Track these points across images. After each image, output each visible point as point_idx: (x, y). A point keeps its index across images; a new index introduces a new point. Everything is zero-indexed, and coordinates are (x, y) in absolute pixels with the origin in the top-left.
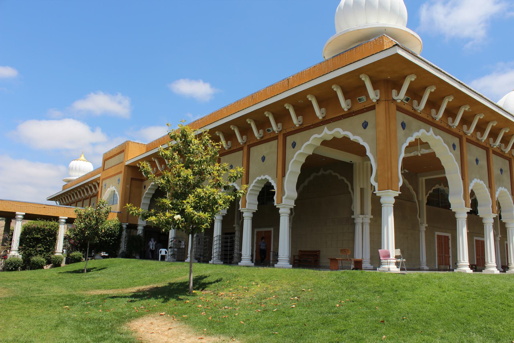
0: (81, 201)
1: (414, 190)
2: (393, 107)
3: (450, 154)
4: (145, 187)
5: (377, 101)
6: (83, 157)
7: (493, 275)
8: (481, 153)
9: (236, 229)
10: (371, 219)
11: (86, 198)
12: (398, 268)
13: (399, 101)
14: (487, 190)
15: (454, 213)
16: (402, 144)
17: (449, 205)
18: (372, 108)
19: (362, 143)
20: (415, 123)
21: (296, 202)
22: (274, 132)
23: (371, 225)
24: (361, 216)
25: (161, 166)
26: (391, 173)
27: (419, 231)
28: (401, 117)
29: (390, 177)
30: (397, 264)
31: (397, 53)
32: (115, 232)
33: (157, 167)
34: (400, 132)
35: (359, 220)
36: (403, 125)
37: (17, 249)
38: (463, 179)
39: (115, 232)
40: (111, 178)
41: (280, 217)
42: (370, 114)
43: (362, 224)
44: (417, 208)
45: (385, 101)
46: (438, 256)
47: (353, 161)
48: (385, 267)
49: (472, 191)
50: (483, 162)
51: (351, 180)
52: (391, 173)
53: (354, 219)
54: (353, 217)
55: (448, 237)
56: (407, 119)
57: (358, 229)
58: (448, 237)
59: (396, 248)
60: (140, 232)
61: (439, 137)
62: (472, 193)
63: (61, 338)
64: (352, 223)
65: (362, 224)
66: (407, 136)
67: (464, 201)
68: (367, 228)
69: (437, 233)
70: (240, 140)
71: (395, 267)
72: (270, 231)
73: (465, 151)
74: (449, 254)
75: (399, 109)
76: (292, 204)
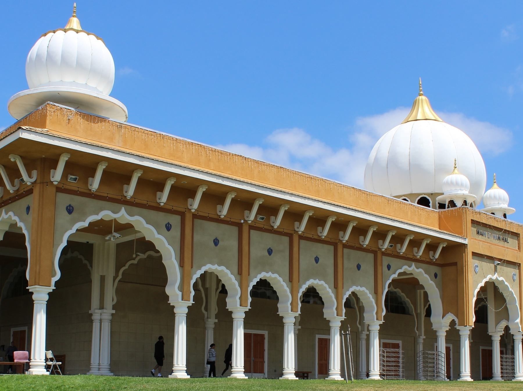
5: (32, 183)
12: (48, 371)
15: (173, 307)
17: (167, 297)
18: (30, 192)
24: (100, 311)
26: (40, 267)
27: (205, 328)
28: (64, 199)
29: (38, 271)
30: (48, 367)
34: (63, 216)
35: (96, 317)
37: (106, 361)
40: (194, 226)
42: (30, 197)
43: (101, 320)
44: (202, 298)
45: (40, 183)
46: (319, 364)
47: (91, 242)
52: (40, 267)
54: (114, 312)
55: (262, 336)
56: (76, 200)
57: (96, 326)
58: (262, 336)
59: (47, 349)
65: (101, 320)
71: (45, 370)
72: (25, 331)
74: (263, 357)
75: (59, 189)
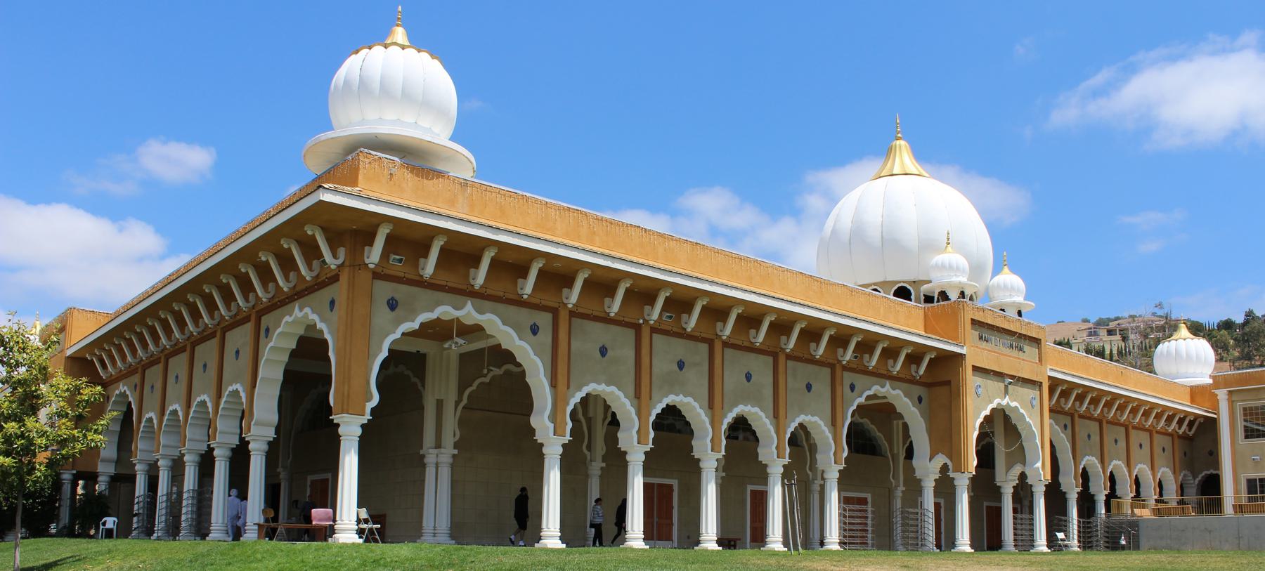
0: (183, 350)
2: (365, 277)
4: (267, 330)
5: (339, 266)
6: (400, 34)
7: (775, 554)
9: (281, 476)
10: (454, 456)
11: (153, 362)
13: (371, 266)
16: (387, 335)
18: (335, 279)
19: (327, 336)
20: (424, 295)
23: (453, 466)
24: (436, 451)
25: (287, 278)
28: (384, 290)
31: (321, 201)
32: (42, 489)
33: (275, 280)
35: (430, 459)
39: (42, 489)
41: (249, 456)
42: (335, 287)
43: (437, 464)
48: (703, 546)
51: (422, 379)
53: (423, 456)
54: (456, 452)
56: (401, 291)
57: (430, 473)
60: (103, 488)
64: (419, 463)
65: (437, 464)
66: (399, 322)
67: (551, 426)
68: (445, 473)
70: (328, 256)
72: (327, 480)
75: (377, 275)
76: (270, 434)
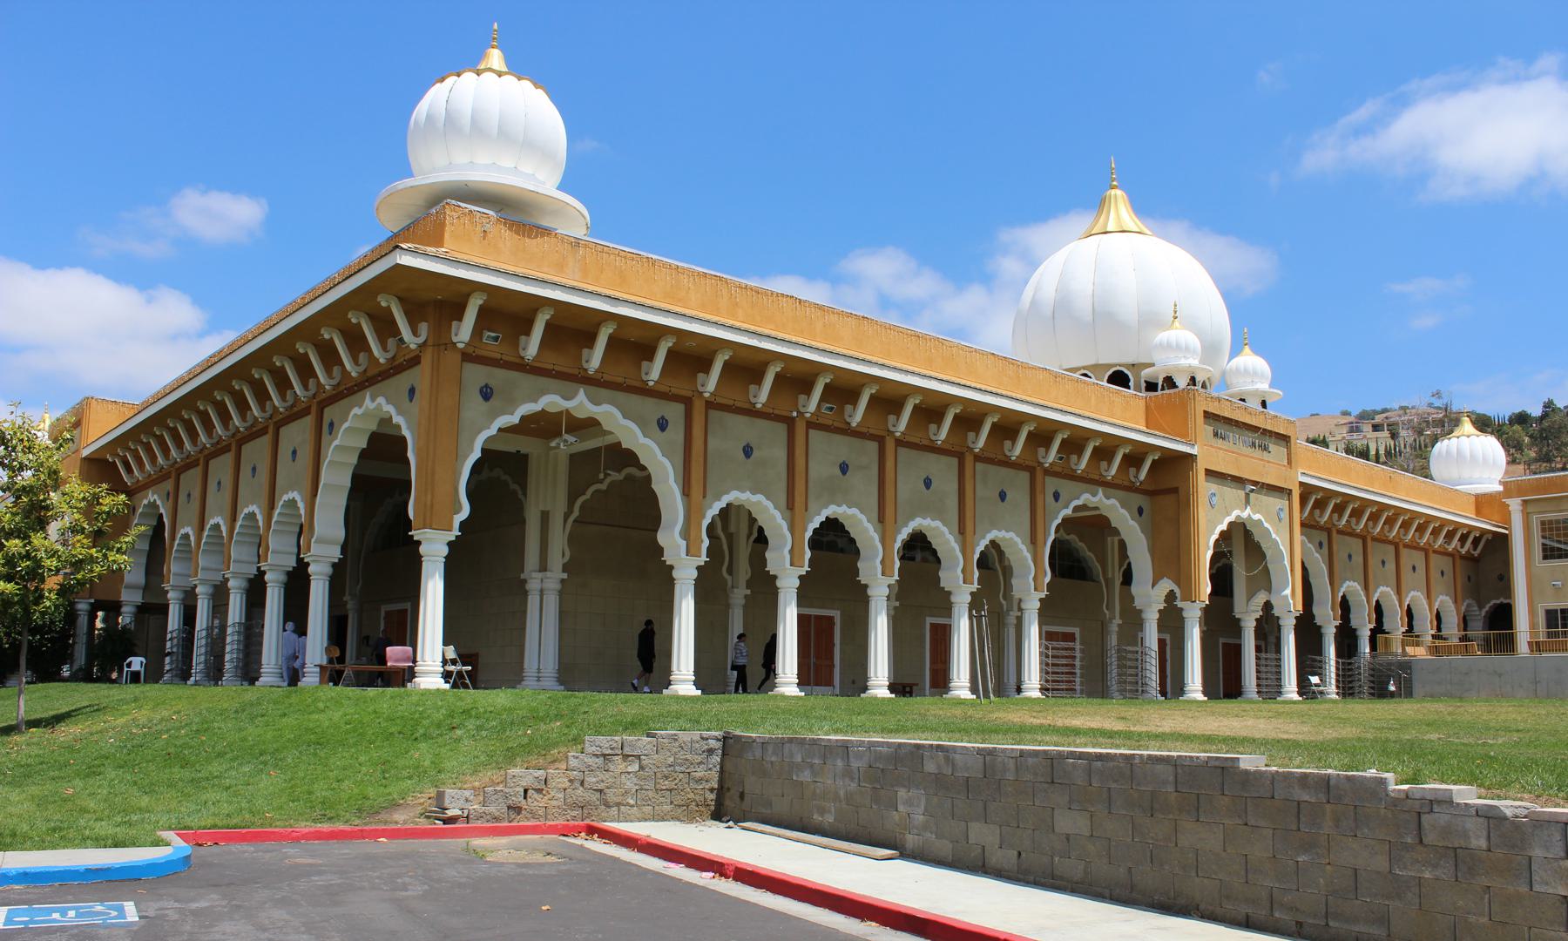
1: (718, 538)
3: (1132, 523)
8: (1418, 558)
10: (563, 581)
14: (1425, 602)
17: (660, 550)
18: (415, 361)
21: (344, 549)
22: (256, 419)
24: (540, 575)
27: (728, 606)
28: (476, 375)
32: (52, 622)
34: (474, 405)
35: (533, 585)
36: (486, 393)
38: (1331, 583)
39: (52, 622)
42: (416, 370)
49: (1344, 597)
50: (1358, 559)
53: (525, 581)
56: (497, 377)
57: (533, 602)
60: (128, 620)
61: (1113, 501)
62: (1344, 599)
63: (227, 788)
64: (520, 590)
66: (494, 415)
69: (929, 620)
73: (1335, 547)
75: (467, 357)
76: (335, 553)
